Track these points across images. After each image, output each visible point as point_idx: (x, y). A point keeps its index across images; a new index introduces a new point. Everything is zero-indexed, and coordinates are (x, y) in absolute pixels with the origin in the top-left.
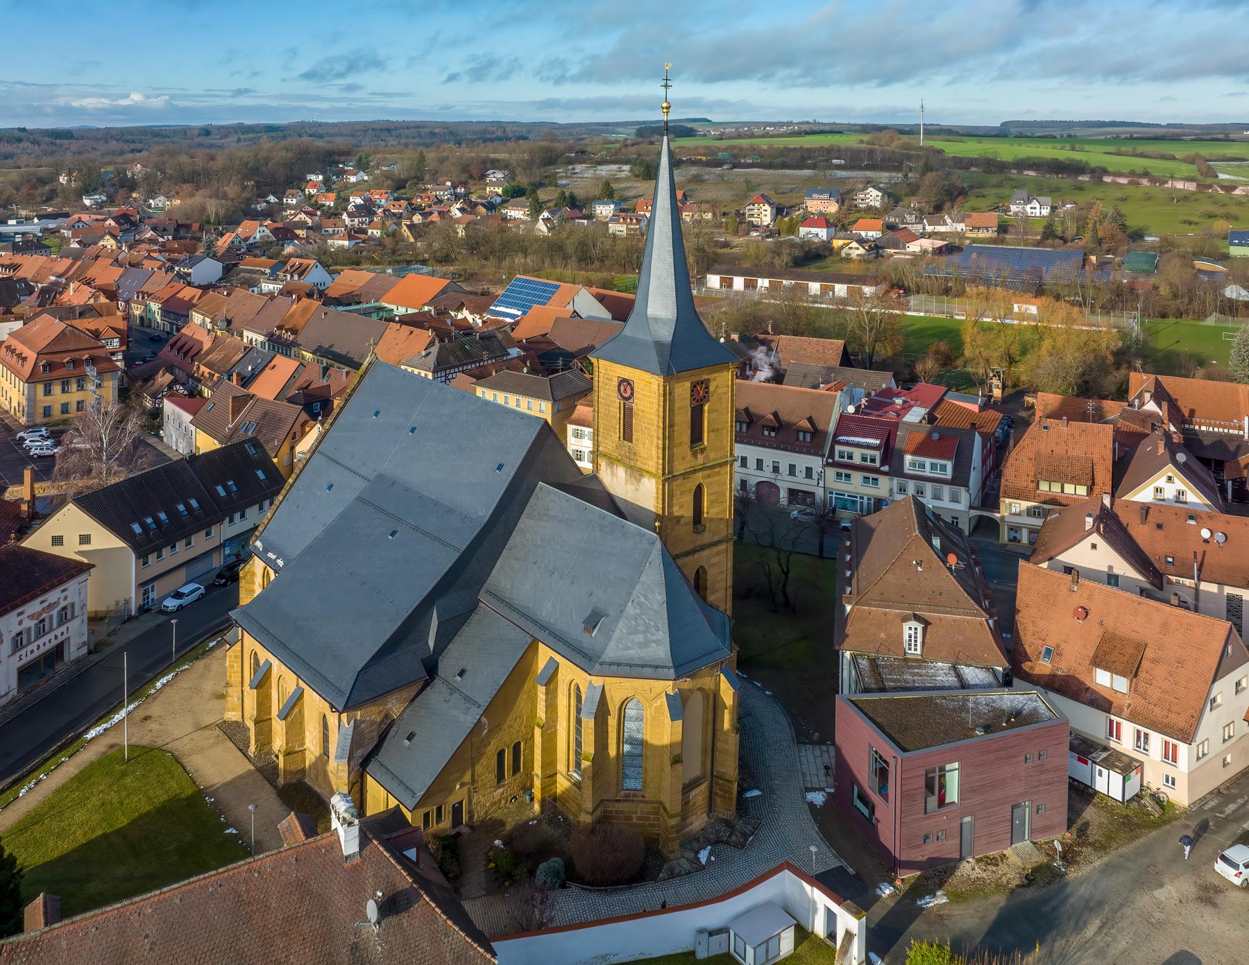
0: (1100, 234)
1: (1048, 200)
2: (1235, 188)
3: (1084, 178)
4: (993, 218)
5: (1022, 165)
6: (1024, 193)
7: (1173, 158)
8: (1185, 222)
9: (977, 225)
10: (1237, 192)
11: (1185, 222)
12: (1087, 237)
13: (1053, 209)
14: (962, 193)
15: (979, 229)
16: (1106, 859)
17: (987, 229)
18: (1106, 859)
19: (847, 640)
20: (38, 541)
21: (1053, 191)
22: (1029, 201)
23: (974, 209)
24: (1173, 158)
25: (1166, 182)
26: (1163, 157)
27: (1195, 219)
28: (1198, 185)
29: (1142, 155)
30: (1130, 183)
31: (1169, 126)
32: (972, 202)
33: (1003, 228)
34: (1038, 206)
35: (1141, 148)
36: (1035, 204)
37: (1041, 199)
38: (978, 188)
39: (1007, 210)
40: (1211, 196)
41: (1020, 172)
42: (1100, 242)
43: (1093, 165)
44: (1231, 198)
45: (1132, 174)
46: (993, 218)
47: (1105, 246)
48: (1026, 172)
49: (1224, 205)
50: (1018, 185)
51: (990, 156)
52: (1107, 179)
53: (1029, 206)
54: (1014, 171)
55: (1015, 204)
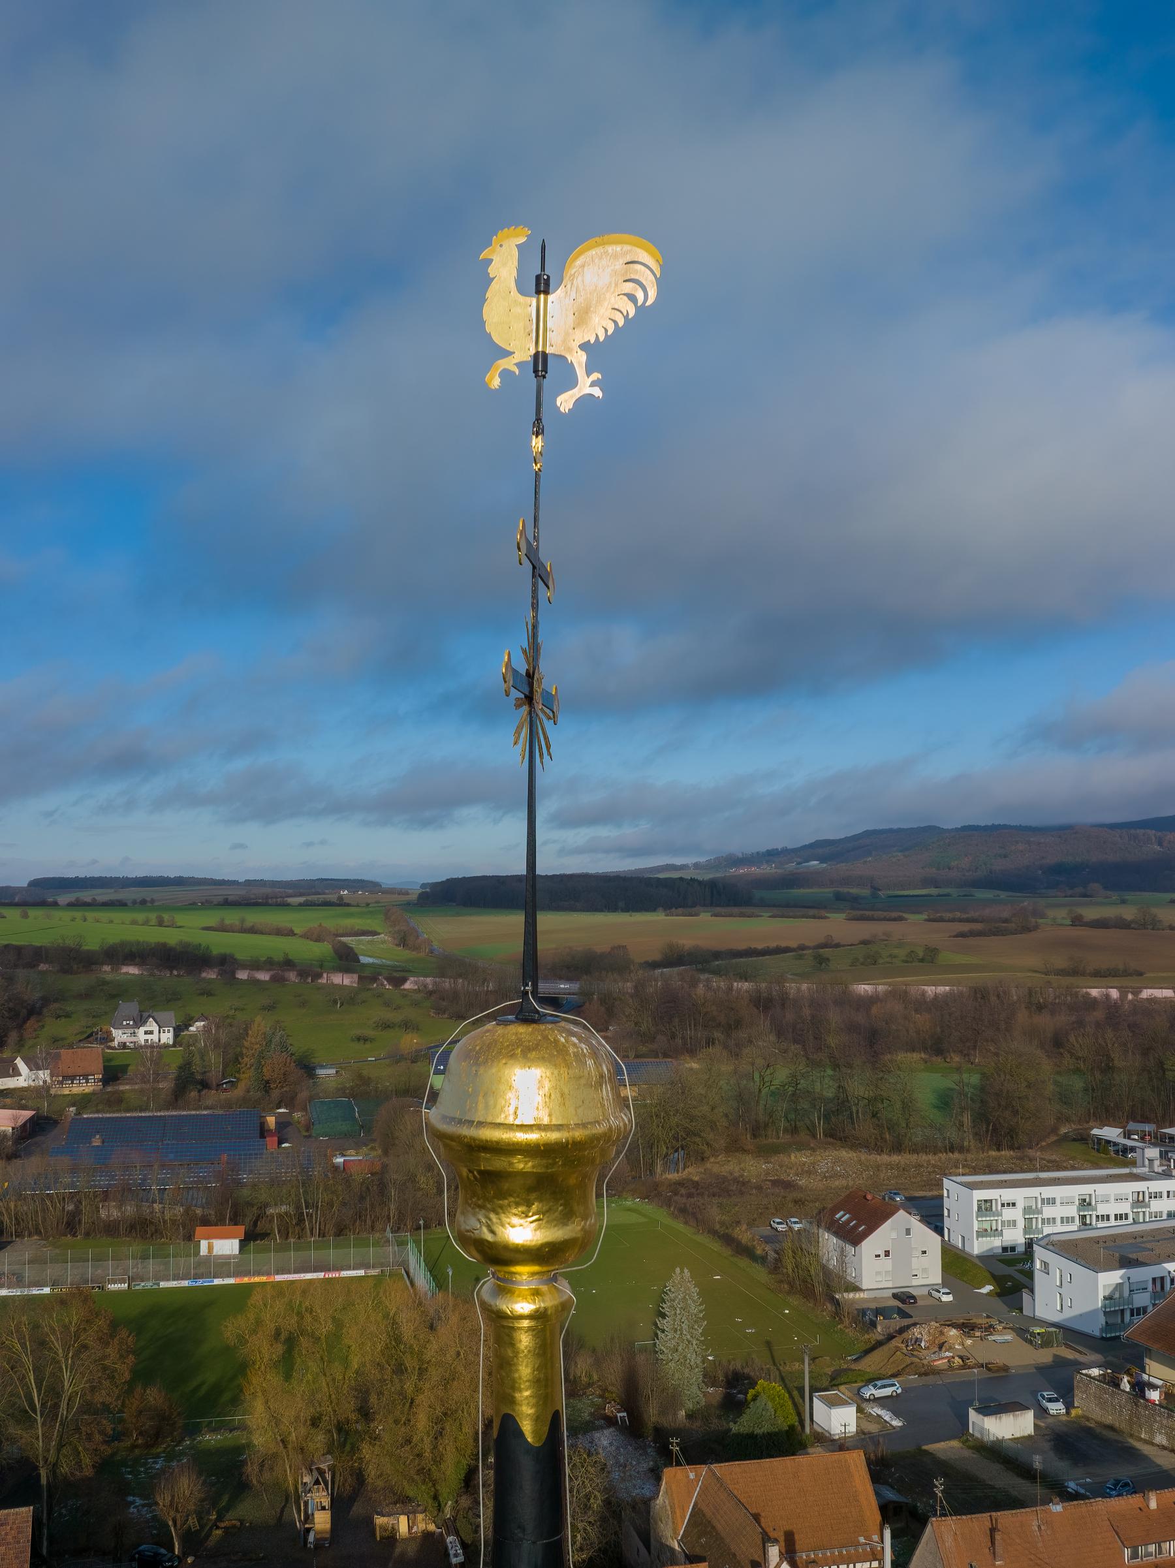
0: (267, 1073)
1: (170, 1016)
2: (404, 980)
3: (211, 975)
4: (92, 1057)
5: (119, 954)
6: (129, 1007)
7: (291, 933)
8: (359, 1039)
9: (70, 1072)
10: (407, 985)
11: (359, 1039)
12: (246, 1081)
13: (178, 1031)
14: (34, 1011)
15: (72, 1078)
16: (1022, 905)
17: (86, 1077)
18: (1022, 905)
19: (796, 1537)
20: (533, 1323)
21: (170, 999)
22: (140, 1021)
23: (56, 1041)
24: (291, 933)
25: (320, 976)
26: (279, 932)
27: (370, 1033)
28: (360, 978)
29: (252, 930)
30: (274, 979)
31: (248, 883)
32: (53, 1027)
33: (112, 1074)
34: (155, 1028)
35: (254, 917)
36: (152, 1025)
37: (161, 1015)
38: (56, 1000)
39: (109, 1038)
40: (379, 996)
41: (115, 969)
42: (266, 1086)
43: (215, 951)
44: (405, 996)
45: (269, 964)
46: (92, 1057)
47: (275, 1094)
48: (125, 969)
49: (398, 1008)
50: (116, 993)
51: (70, 943)
52: (242, 975)
53: (142, 1029)
54: (107, 968)
55: (119, 1026)
